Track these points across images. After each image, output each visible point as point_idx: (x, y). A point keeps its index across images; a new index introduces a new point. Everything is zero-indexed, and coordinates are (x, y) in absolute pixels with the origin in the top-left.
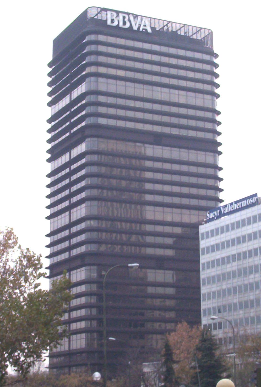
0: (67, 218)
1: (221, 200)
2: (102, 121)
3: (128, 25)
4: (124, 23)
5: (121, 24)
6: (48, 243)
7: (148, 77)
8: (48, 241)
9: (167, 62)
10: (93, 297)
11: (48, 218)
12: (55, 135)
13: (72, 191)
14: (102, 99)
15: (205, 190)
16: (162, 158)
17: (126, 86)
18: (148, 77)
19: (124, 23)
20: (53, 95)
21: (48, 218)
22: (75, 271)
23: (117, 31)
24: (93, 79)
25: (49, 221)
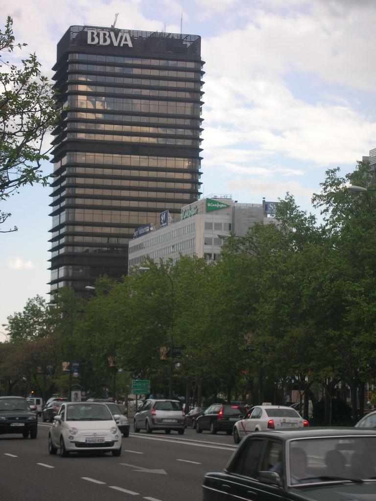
0: (62, 163)
1: (201, 129)
2: (81, 136)
3: (108, 42)
4: (105, 40)
5: (101, 43)
6: (50, 238)
7: (116, 203)
8: (50, 236)
9: (149, 74)
10: (69, 237)
11: (52, 215)
12: (58, 147)
13: (61, 206)
14: (80, 170)
15: (173, 194)
16: (121, 166)
17: (95, 156)
18: (116, 203)
19: (105, 40)
20: (57, 144)
21: (52, 215)
22: (69, 134)
23: (98, 50)
24: (71, 210)
25: (51, 217)
